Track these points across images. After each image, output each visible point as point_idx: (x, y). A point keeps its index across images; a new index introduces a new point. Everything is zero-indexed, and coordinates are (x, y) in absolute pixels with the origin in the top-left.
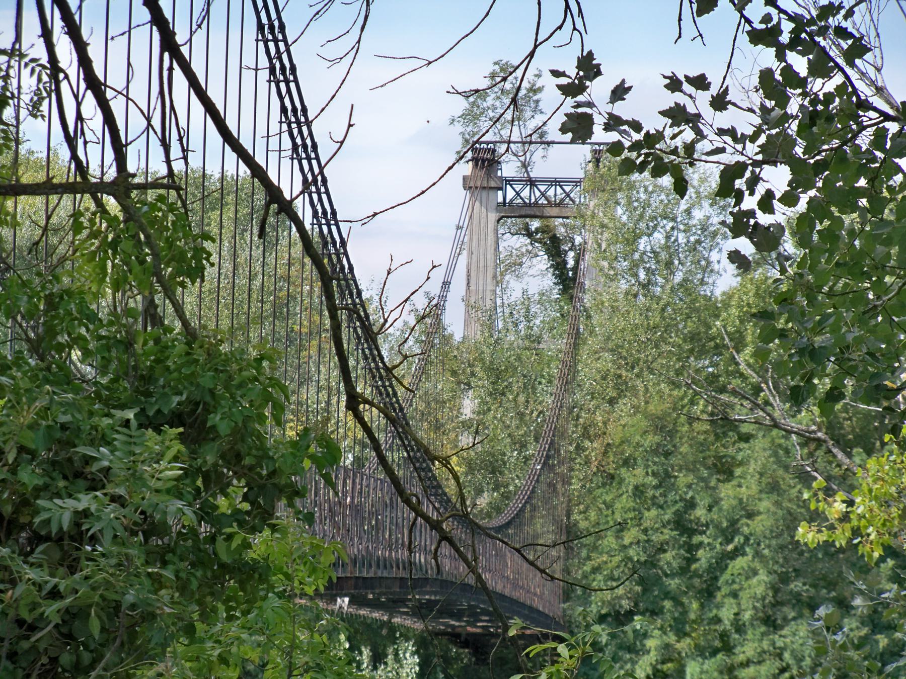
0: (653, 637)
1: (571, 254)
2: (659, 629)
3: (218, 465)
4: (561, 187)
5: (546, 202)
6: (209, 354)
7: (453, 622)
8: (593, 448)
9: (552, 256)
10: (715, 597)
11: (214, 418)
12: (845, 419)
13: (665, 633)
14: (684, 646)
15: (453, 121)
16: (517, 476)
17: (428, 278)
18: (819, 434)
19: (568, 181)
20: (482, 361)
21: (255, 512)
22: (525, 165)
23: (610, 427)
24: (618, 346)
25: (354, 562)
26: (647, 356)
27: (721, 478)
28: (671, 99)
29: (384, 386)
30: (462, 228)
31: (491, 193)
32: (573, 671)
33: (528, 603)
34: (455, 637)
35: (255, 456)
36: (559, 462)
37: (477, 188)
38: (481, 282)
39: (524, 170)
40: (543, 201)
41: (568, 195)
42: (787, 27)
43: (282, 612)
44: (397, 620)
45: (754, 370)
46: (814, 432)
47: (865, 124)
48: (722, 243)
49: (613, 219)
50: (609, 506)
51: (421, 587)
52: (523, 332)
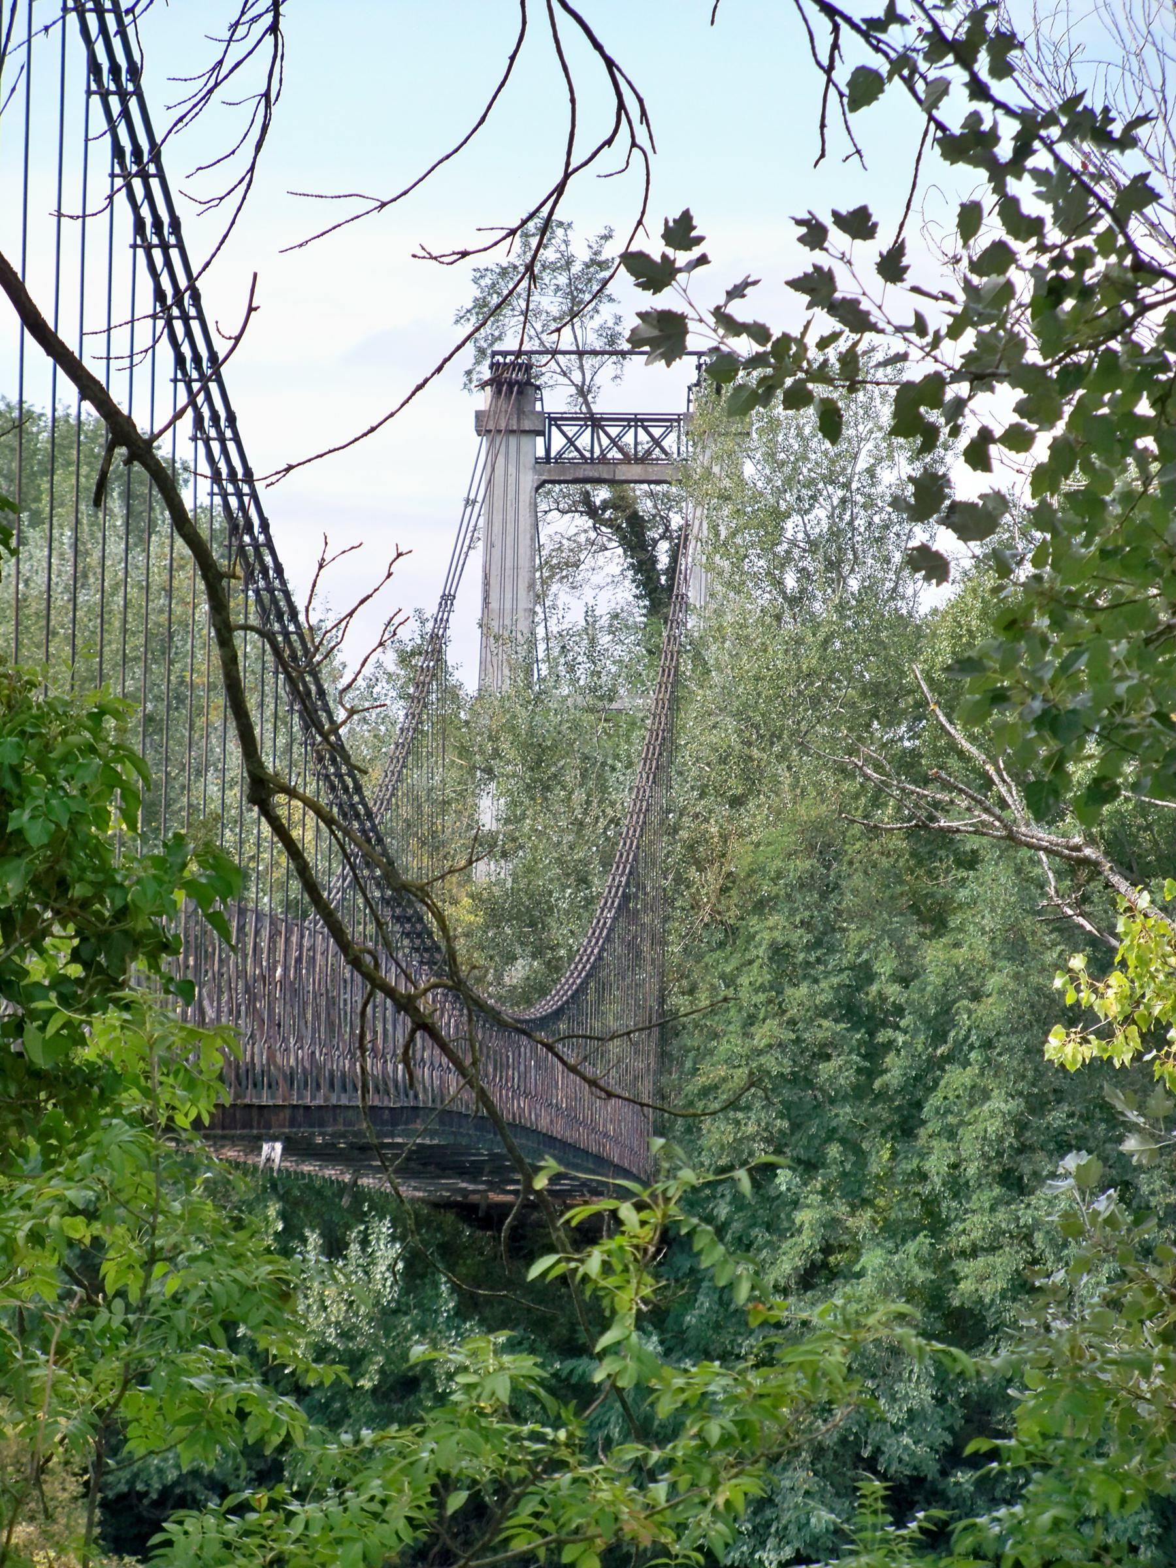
0: (808, 1206)
1: (664, 546)
2: (818, 1193)
3: (27, 899)
4: (645, 428)
5: (620, 456)
6: (10, 707)
7: (464, 1185)
8: (707, 882)
9: (632, 549)
10: (916, 1137)
11: (21, 816)
12: (1140, 828)
13: (830, 1202)
14: (862, 1221)
16: (572, 932)
17: (390, 575)
18: (1088, 851)
19: (658, 420)
20: (513, 729)
21: (91, 981)
22: (583, 392)
23: (734, 844)
25: (291, 1078)
26: (799, 723)
27: (928, 931)
28: (805, 260)
29: (340, 776)
30: (474, 502)
31: (525, 441)
32: (646, 1250)
33: (594, 1149)
34: (467, 1211)
35: (92, 883)
36: (645, 906)
37: (499, 431)
38: (509, 595)
39: (581, 400)
40: (614, 454)
41: (657, 443)
42: (1009, 128)
43: (135, 1149)
44: (367, 1182)
45: (980, 747)
46: (1078, 848)
47: (1148, 301)
49: (741, 482)
50: (730, 981)
51: (406, 1123)
52: (582, 682)
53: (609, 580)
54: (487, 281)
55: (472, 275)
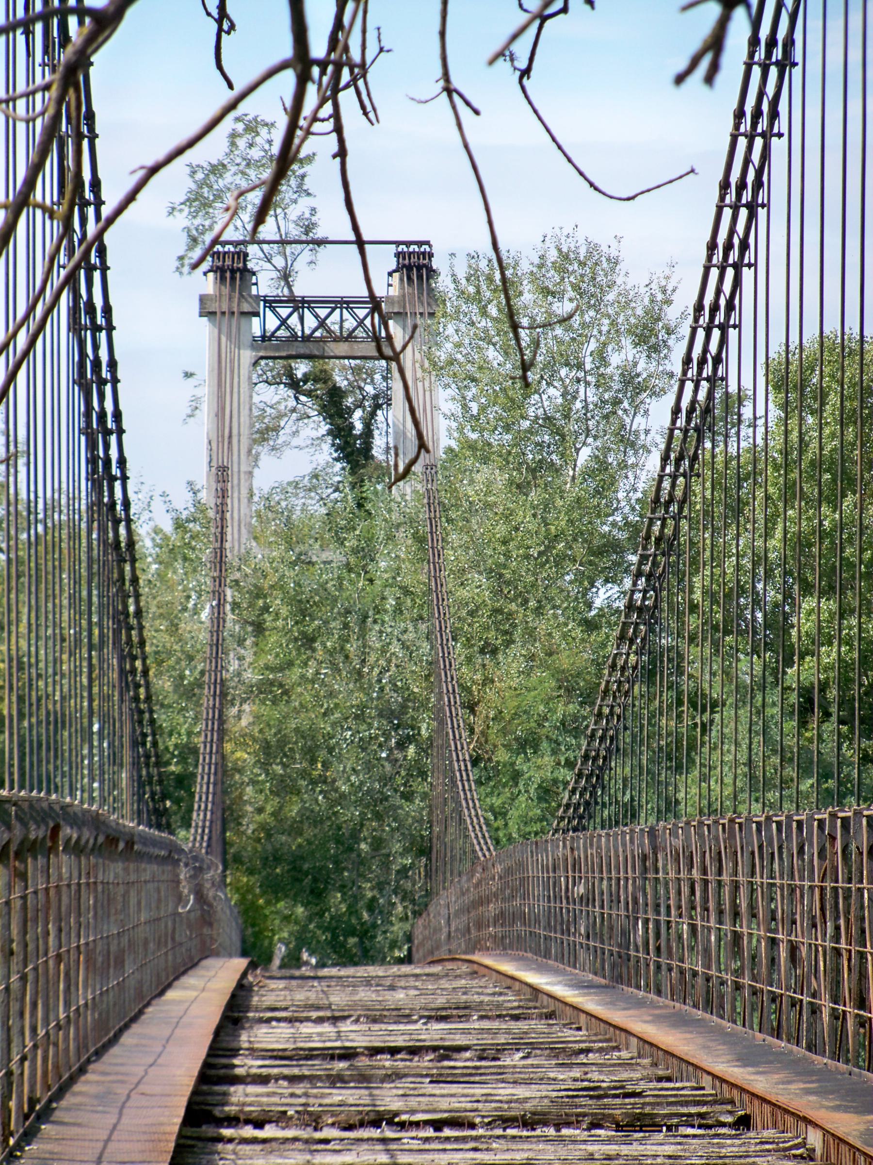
9: (331, 417)
15: (172, 211)
24: (499, 565)
31: (244, 321)
37: (223, 313)
48: (648, 400)
53: (309, 442)
54: (200, 176)
55: (188, 170)
